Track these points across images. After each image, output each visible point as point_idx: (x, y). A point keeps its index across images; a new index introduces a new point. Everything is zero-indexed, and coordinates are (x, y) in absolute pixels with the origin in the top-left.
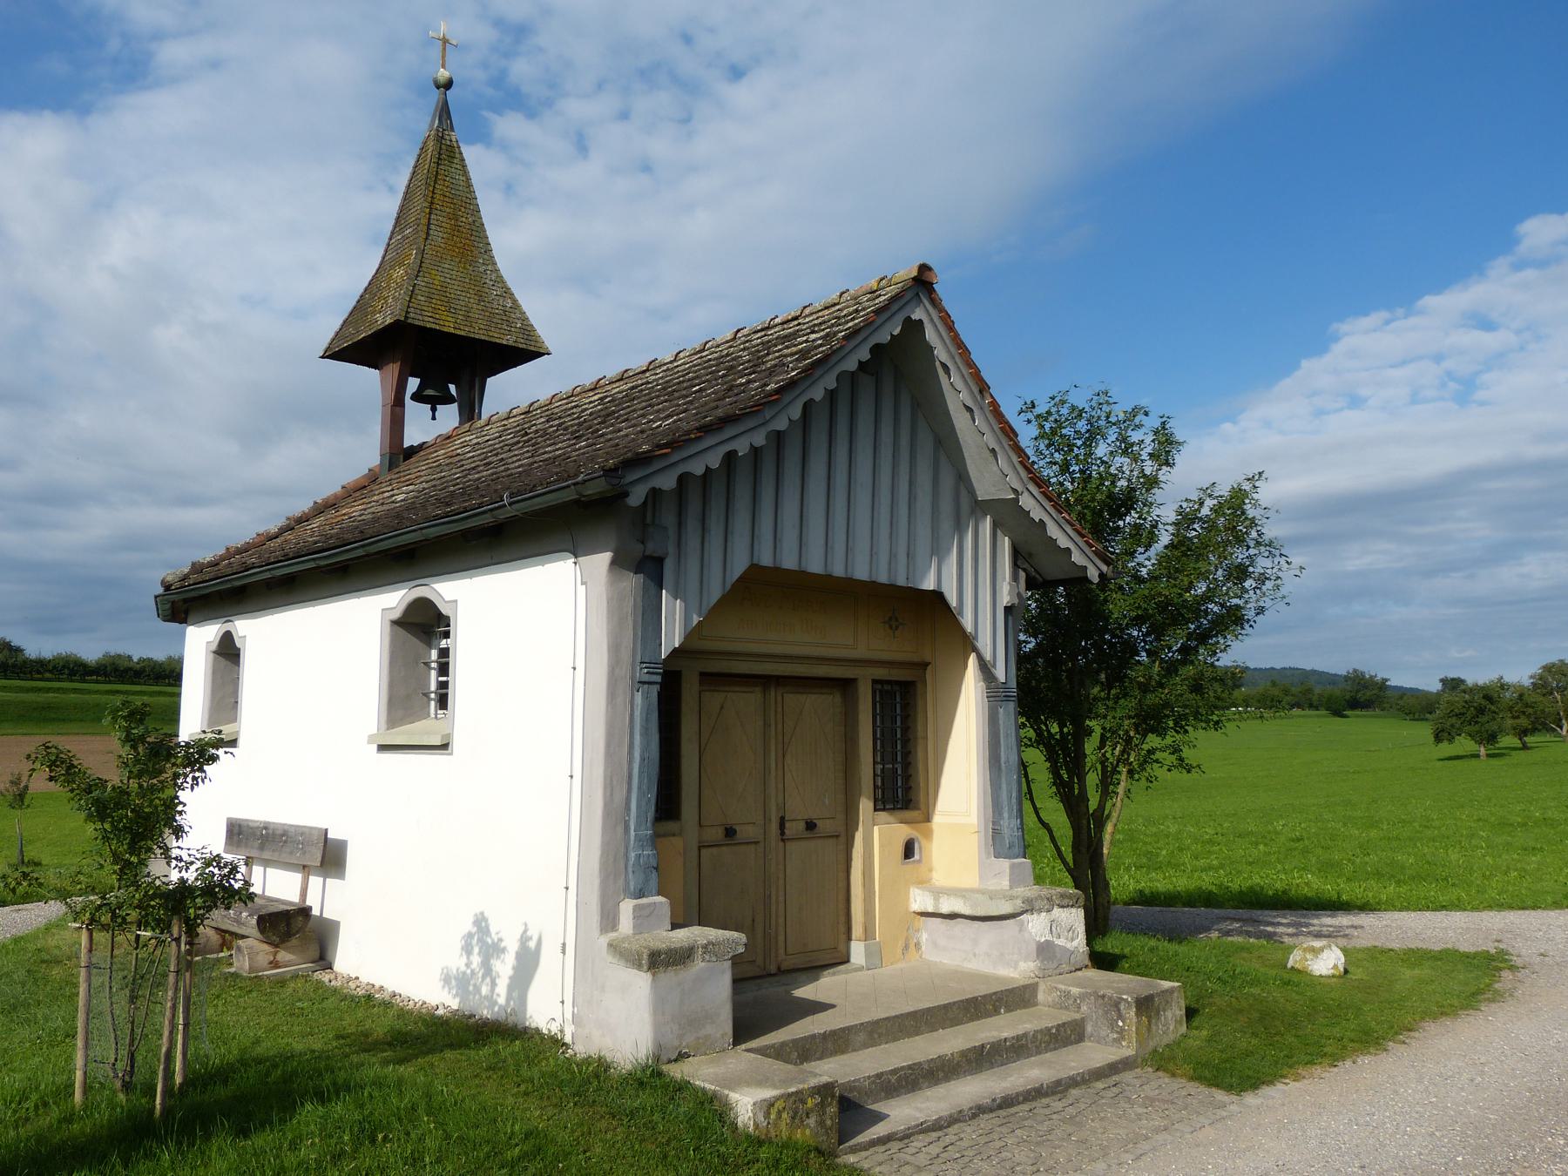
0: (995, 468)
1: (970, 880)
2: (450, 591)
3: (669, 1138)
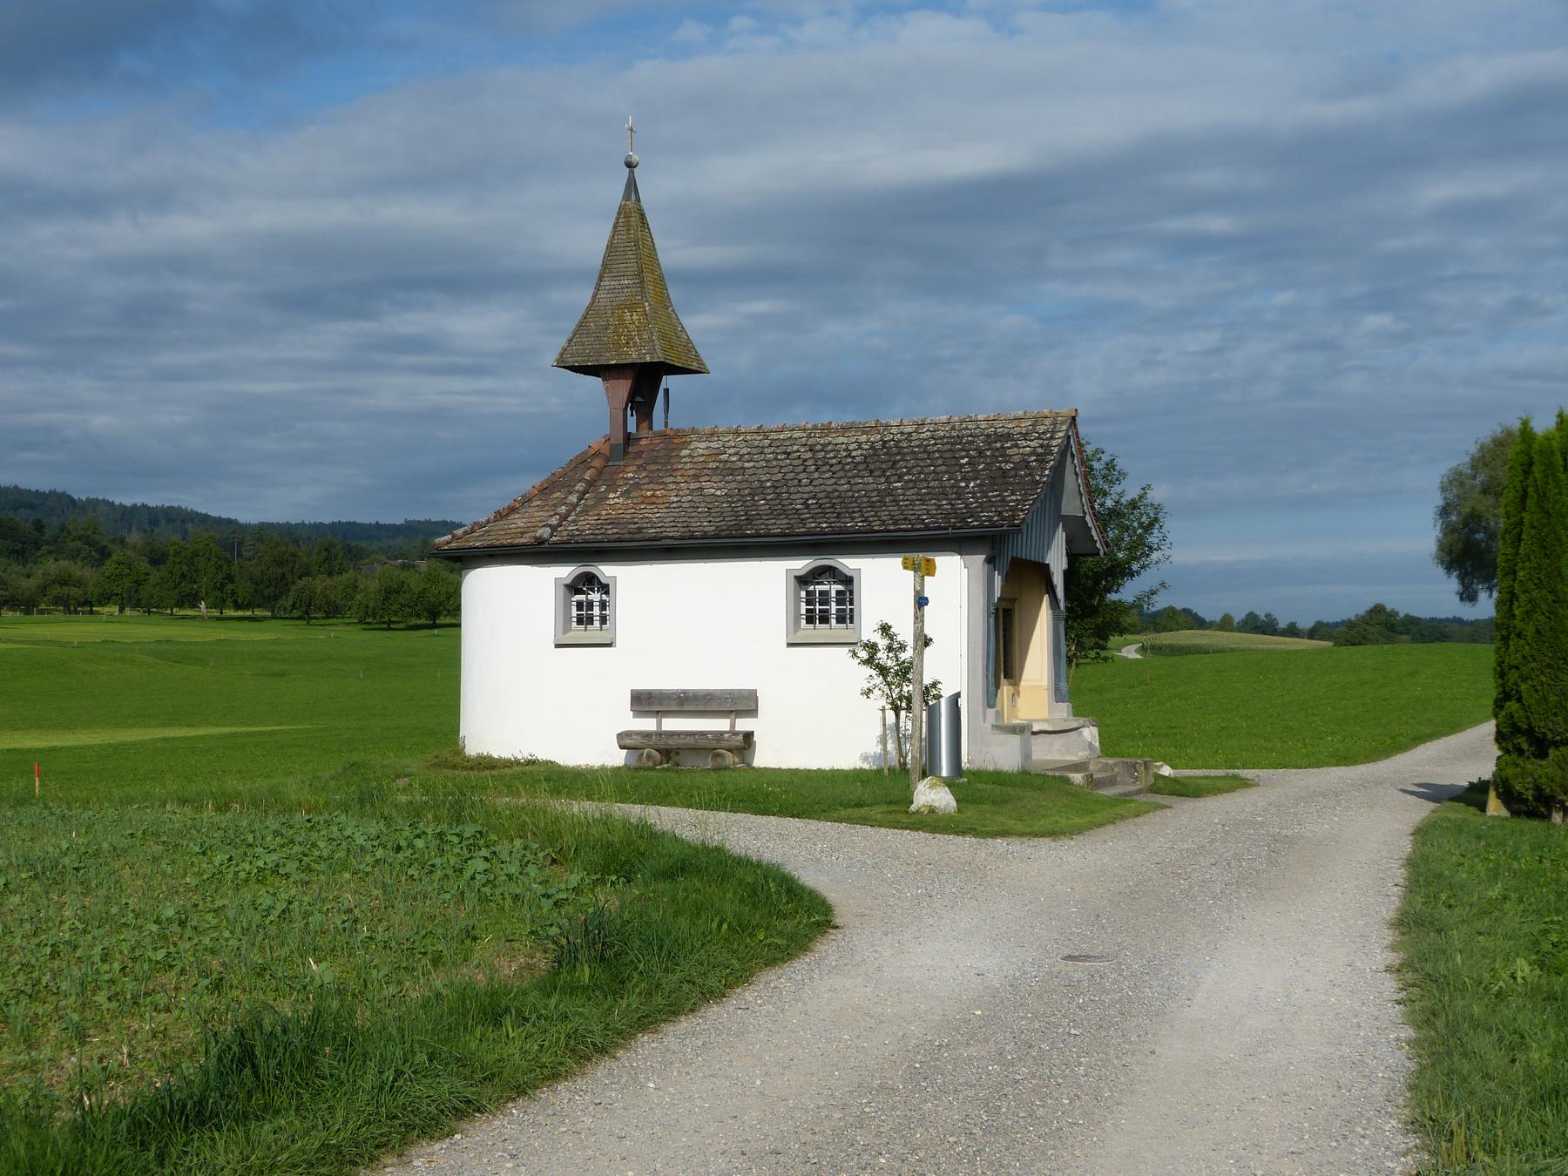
0: (1078, 502)
1: (1045, 715)
2: (606, 571)
3: (162, 1165)
